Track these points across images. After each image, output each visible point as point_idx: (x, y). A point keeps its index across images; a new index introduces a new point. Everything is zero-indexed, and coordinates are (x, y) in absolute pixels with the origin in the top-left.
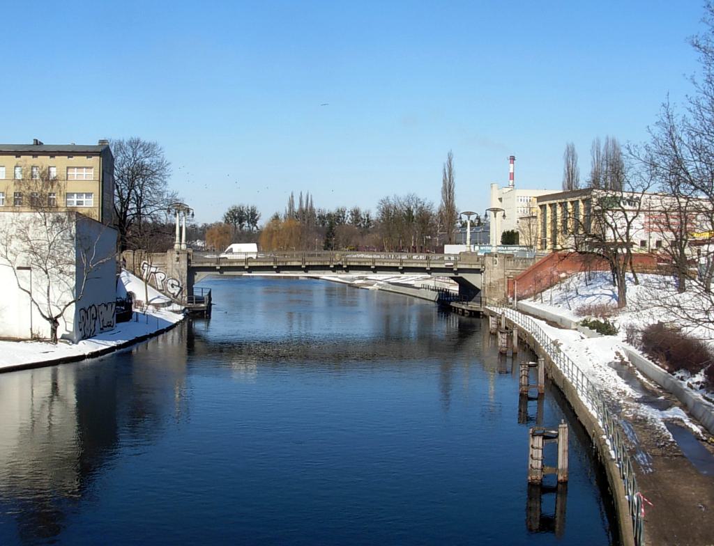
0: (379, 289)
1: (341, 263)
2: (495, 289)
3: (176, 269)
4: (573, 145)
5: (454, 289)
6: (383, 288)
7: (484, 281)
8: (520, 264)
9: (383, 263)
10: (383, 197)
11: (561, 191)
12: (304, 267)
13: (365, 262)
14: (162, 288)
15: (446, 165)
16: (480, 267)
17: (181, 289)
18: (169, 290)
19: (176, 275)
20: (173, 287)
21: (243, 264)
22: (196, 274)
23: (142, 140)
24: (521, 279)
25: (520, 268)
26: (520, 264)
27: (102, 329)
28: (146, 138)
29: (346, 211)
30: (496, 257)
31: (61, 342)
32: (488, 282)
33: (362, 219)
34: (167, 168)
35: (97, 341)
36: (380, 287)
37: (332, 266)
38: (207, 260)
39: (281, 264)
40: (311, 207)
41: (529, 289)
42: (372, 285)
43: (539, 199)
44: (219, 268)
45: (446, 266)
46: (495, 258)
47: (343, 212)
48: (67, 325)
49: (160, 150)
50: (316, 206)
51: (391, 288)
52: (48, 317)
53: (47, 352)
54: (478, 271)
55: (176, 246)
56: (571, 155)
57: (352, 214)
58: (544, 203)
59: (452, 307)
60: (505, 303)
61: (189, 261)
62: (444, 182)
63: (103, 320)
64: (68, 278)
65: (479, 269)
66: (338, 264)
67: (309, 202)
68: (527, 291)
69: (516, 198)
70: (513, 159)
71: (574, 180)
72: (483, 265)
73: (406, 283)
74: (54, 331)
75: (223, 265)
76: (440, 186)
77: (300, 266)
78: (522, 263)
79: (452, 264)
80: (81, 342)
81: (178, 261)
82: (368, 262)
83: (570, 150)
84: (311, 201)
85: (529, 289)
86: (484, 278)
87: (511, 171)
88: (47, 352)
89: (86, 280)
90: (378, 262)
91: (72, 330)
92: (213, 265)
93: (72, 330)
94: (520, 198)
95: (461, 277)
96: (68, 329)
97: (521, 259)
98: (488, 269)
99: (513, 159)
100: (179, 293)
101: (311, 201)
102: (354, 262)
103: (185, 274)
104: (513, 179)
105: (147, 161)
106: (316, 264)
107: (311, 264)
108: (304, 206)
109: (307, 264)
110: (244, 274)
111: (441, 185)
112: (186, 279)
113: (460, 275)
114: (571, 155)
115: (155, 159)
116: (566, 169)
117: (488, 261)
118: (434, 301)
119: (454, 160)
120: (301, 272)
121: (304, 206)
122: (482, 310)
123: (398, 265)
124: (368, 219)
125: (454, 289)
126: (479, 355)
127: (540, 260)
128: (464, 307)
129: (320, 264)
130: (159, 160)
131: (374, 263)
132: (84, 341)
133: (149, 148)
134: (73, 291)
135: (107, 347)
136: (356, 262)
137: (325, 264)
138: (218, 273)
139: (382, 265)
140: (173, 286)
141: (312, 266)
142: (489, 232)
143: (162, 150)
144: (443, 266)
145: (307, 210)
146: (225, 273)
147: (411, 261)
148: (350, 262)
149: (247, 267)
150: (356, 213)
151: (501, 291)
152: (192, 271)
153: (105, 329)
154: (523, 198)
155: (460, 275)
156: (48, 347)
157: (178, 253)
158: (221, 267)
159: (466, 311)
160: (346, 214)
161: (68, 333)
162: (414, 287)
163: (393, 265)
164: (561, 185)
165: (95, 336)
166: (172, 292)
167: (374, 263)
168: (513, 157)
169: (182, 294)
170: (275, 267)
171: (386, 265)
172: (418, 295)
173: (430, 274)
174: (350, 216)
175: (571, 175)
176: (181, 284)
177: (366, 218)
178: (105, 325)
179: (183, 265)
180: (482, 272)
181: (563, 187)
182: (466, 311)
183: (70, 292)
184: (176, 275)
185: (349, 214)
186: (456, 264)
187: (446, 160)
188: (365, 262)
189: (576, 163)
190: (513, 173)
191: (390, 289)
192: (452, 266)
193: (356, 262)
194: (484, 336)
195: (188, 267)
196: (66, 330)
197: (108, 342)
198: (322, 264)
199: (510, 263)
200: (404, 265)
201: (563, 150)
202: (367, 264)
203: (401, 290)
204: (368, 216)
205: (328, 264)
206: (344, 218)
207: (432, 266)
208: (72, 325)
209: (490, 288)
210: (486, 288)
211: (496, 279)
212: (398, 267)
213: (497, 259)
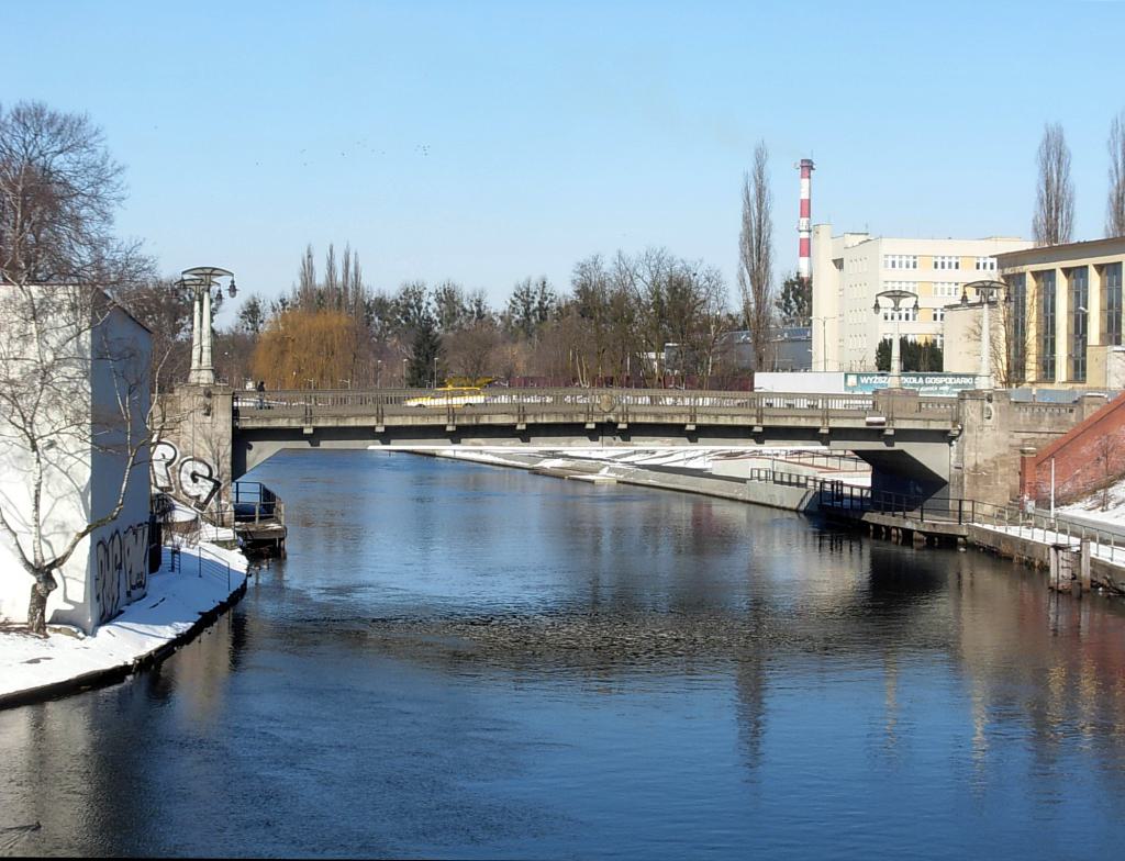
0: (619, 482)
1: (613, 418)
2: (988, 480)
3: (205, 437)
4: (1060, 129)
5: (858, 478)
6: (632, 479)
7: (961, 459)
8: (1047, 418)
9: (717, 416)
10: (584, 256)
11: (1030, 245)
12: (382, 429)
13: (672, 415)
14: (167, 485)
15: (751, 179)
16: (949, 427)
17: (218, 484)
18: (186, 488)
19: (204, 450)
20: (195, 481)
21: (443, 421)
22: (250, 447)
23: (50, 109)
24: (1059, 451)
25: (1047, 430)
26: (1047, 418)
27: (129, 594)
28: (60, 103)
29: (425, 292)
30: (990, 400)
31: (56, 630)
32: (969, 463)
33: (465, 310)
34: (116, 179)
35: (119, 623)
36: (621, 477)
37: (591, 426)
38: (408, 411)
39: (465, 421)
40: (357, 286)
41: (1074, 479)
42: (596, 472)
43: (1004, 260)
44: (310, 431)
45: (868, 424)
46: (986, 404)
47: (418, 295)
48: (73, 587)
49: (96, 133)
50: (365, 282)
51: (652, 479)
52: (31, 560)
53: (36, 661)
54: (944, 437)
55: (193, 378)
56: (1054, 154)
57: (439, 300)
58: (1019, 269)
59: (868, 524)
60: (1015, 512)
61: (235, 413)
62: (747, 221)
63: (130, 572)
64: (70, 460)
65: (947, 432)
66: (605, 419)
67: (352, 269)
68: (1069, 485)
69: (882, 260)
70: (808, 166)
71: (1063, 216)
72: (955, 422)
73: (681, 464)
74: (39, 601)
75: (321, 424)
76: (737, 227)
77: (513, 426)
78: (1051, 415)
79: (883, 419)
80: (103, 630)
81: (208, 414)
82: (680, 415)
83: (1052, 142)
84: (356, 268)
85: (1074, 479)
86: (960, 452)
87: (805, 196)
88: (36, 661)
89: (133, 465)
90: (702, 414)
91: (80, 598)
92: (295, 424)
93: (81, 600)
94: (890, 259)
95: (901, 452)
96: (70, 597)
97: (1049, 405)
98: (970, 430)
99: (808, 166)
100: (211, 495)
101: (356, 268)
102: (646, 414)
103: (226, 448)
104: (809, 217)
105: (59, 162)
106: (552, 420)
107: (539, 421)
108: (340, 278)
109: (530, 420)
110: (371, 448)
111: (739, 227)
112: (229, 460)
113: (898, 446)
114: (1054, 154)
115: (85, 156)
116: (1043, 188)
117: (971, 410)
118: (797, 511)
119: (769, 167)
120: (513, 441)
121: (340, 278)
122: (965, 532)
123: (753, 422)
124: (479, 311)
125: (858, 478)
126: (949, 646)
127: (1095, 408)
128: (909, 525)
129: (561, 420)
130: (96, 159)
131: (693, 417)
132: (106, 627)
133: (68, 131)
134: (83, 496)
135: (163, 642)
136: (651, 414)
137: (575, 420)
138: (306, 445)
139: (712, 421)
140: (194, 477)
141: (542, 425)
142: (809, 340)
143: (102, 135)
144: (861, 424)
145: (346, 289)
146: (324, 445)
147: (792, 412)
148: (635, 414)
149: (380, 429)
150: (448, 298)
151: (1006, 482)
152: (242, 439)
153: (134, 593)
154: (897, 260)
155: (898, 446)
156: (30, 646)
157: (209, 395)
158: (315, 429)
159: (916, 535)
160: (425, 299)
161: (70, 607)
162: (711, 476)
163: (740, 421)
164: (1030, 227)
165: (121, 612)
166: (193, 494)
167: (693, 417)
168: (809, 161)
169: (219, 498)
170: (449, 429)
171: (722, 421)
172: (740, 496)
173: (828, 444)
174: (435, 305)
175: (1055, 203)
176: (215, 474)
177: (475, 309)
178: (134, 584)
179: (222, 425)
180: (953, 438)
181: (1106, 230)
182: (916, 535)
183: (77, 498)
184: (204, 450)
185: (432, 299)
186: (891, 419)
187: (749, 166)
188: (672, 415)
189: (1067, 170)
190: (809, 200)
191: (651, 482)
192: (883, 424)
193: (651, 414)
194: (309, 589)
195: (235, 429)
196: (66, 600)
197: (157, 628)
198: (568, 421)
199: (1024, 416)
200: (766, 422)
201: (1037, 140)
202: (677, 420)
203: (683, 482)
204: (479, 303)
205: (581, 420)
206: (420, 309)
207: (388, 421)
208: (83, 586)
209: (975, 480)
210: (966, 478)
211: (989, 456)
212: (751, 427)
213: (991, 406)
